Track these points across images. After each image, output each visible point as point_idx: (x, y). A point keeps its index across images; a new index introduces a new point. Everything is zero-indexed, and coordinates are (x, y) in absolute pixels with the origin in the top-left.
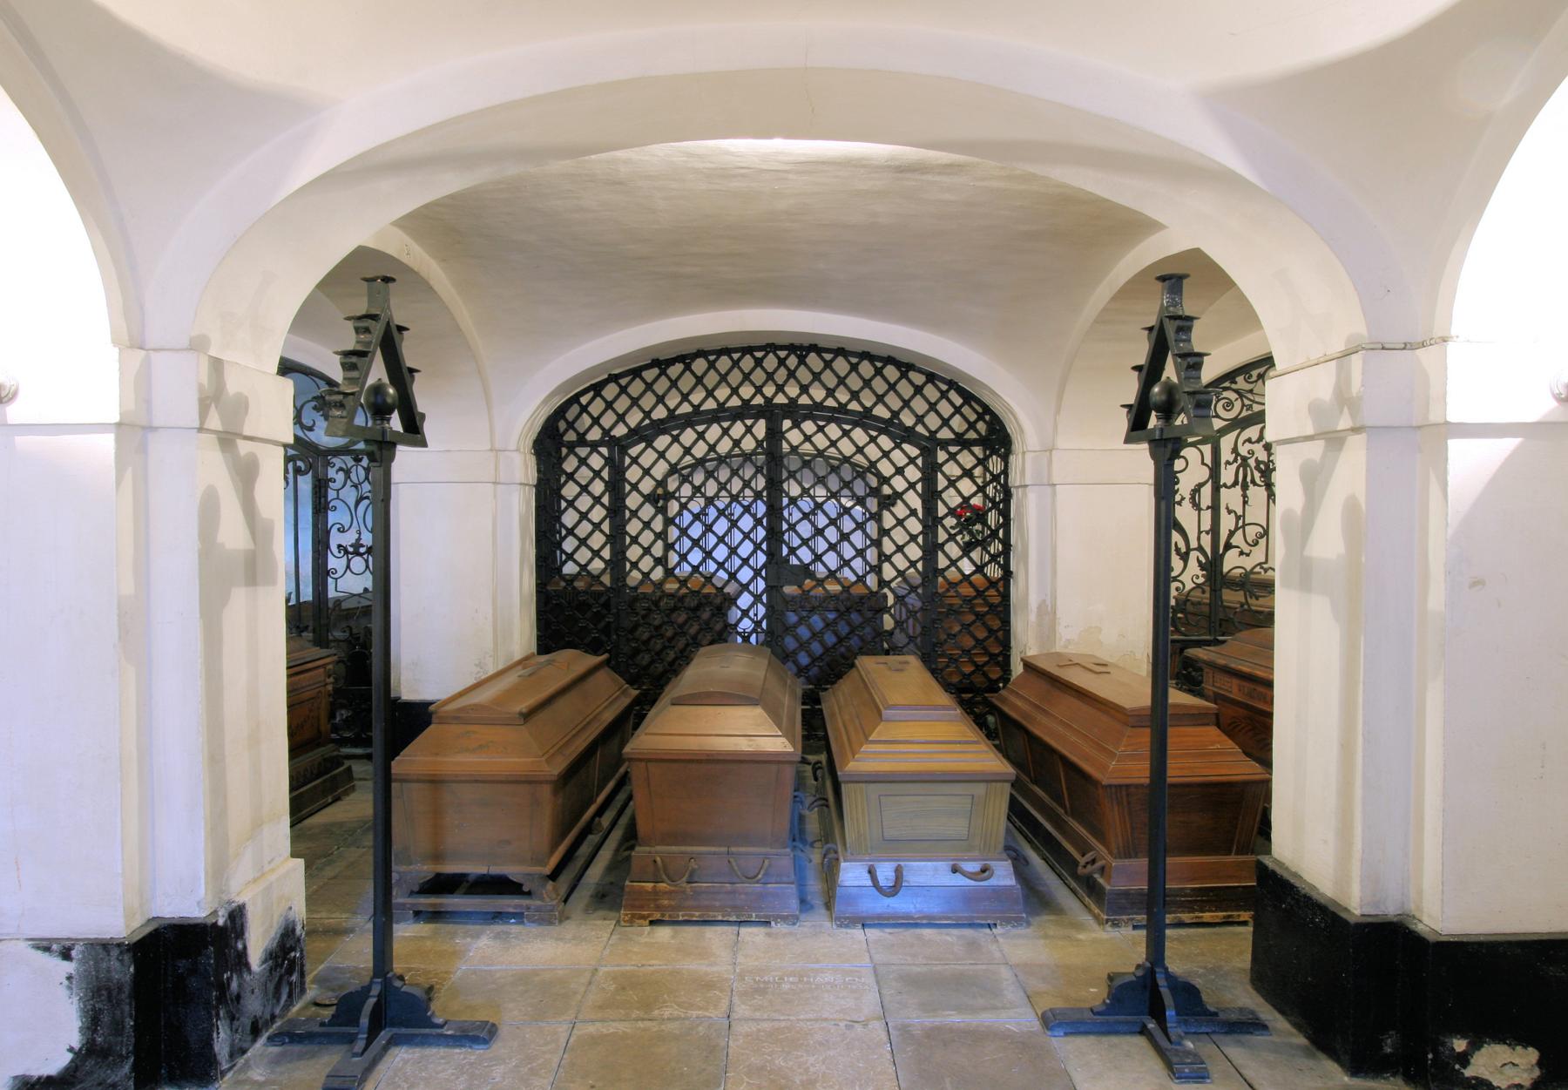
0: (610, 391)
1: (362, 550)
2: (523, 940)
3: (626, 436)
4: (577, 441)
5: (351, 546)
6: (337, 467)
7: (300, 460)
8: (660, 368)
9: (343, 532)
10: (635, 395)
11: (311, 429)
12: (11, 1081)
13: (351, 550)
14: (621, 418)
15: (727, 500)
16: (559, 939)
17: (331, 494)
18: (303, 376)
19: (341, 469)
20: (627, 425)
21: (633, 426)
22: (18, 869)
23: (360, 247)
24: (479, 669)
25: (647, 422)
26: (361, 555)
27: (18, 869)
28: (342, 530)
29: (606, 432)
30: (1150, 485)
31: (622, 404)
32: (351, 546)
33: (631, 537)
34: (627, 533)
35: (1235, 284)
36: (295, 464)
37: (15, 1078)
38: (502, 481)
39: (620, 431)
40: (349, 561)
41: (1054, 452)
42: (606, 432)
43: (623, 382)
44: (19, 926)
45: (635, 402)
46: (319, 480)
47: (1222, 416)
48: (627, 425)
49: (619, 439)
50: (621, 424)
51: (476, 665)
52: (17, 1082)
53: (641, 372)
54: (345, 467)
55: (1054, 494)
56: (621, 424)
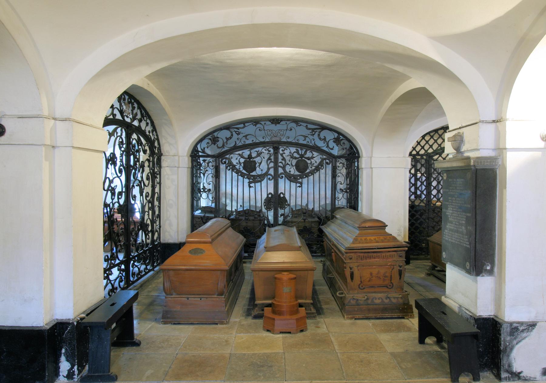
0: (427, 138)
1: (206, 190)
2: (54, 321)
3: (433, 153)
4: (416, 154)
5: (344, 189)
6: (339, 162)
7: (328, 160)
8: (444, 130)
9: (341, 184)
10: (436, 139)
11: (332, 149)
12: (542, 370)
13: (344, 190)
14: (431, 146)
15: (437, 174)
16: (57, 319)
17: (338, 171)
18: (329, 131)
19: (341, 163)
20: (433, 149)
21: (435, 149)
22: (543, 298)
23: (133, 85)
24: (398, 231)
25: (439, 148)
26: (205, 192)
27: (543, 298)
28: (341, 184)
29: (426, 151)
30: (163, 167)
31: (431, 142)
32: (344, 189)
33: (433, 187)
34: (425, 186)
35: (436, 98)
36: (326, 161)
37: (544, 368)
38: (180, 166)
39: (430, 151)
40: (343, 194)
41: (372, 158)
42: (426, 151)
43: (432, 134)
44: (543, 317)
45: (436, 141)
46: (159, 164)
47: (222, 141)
48: (433, 149)
49: (430, 154)
50: (431, 149)
51: (398, 230)
52: (544, 370)
53: (438, 131)
54: (342, 162)
55: (372, 171)
56: (431, 149)
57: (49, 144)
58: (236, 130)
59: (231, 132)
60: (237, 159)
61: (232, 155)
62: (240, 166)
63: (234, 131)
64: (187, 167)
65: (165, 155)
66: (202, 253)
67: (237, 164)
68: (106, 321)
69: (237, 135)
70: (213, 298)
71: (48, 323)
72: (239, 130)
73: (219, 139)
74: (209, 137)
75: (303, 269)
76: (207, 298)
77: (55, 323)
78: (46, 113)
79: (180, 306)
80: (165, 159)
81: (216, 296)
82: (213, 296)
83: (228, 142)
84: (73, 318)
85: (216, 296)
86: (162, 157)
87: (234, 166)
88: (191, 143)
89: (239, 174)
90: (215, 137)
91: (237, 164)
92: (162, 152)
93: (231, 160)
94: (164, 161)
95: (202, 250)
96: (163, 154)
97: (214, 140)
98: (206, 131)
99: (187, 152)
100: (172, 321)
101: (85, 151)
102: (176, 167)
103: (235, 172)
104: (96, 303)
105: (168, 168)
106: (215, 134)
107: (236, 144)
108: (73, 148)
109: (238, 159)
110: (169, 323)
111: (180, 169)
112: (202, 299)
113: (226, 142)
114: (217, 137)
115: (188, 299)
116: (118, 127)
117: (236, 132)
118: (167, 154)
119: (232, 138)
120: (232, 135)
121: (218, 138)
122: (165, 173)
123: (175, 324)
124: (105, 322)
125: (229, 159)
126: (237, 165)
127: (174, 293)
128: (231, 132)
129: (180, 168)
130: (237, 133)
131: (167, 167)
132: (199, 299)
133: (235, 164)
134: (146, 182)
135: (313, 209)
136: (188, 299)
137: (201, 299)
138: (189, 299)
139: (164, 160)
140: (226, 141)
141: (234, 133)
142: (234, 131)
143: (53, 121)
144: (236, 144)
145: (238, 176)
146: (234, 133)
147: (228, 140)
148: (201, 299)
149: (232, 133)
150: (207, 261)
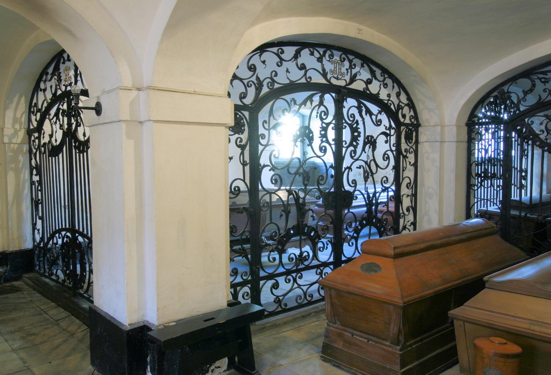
16: (148, 322)
57: (129, 119)
58: (541, 76)
59: (533, 81)
60: (541, 124)
61: (532, 119)
62: (547, 135)
63: (538, 78)
64: (456, 141)
65: (424, 125)
66: (376, 271)
67: (542, 132)
68: (162, 341)
69: (543, 84)
70: (383, 344)
71: (135, 323)
72: (547, 75)
73: (511, 95)
74: (495, 94)
75: (538, 338)
76: (376, 342)
77: (142, 324)
78: (128, 83)
79: (342, 343)
80: (423, 132)
81: (388, 343)
82: (384, 342)
83: (526, 97)
84: (157, 325)
85: (388, 343)
86: (419, 128)
87: (537, 136)
88: (461, 106)
89: (546, 148)
90: (505, 93)
91: (542, 132)
92: (420, 122)
93: (532, 126)
94: (423, 134)
95: (378, 266)
96: (422, 125)
97: (503, 97)
98: (483, 86)
99: (456, 118)
100: (334, 361)
101: (193, 125)
102: (437, 141)
103: (537, 146)
104: (208, 312)
105: (427, 143)
106: (505, 88)
107: (540, 98)
108: (153, 122)
109: (544, 125)
110: (329, 362)
111: (446, 144)
112: (370, 342)
113: (524, 98)
114: (508, 92)
115: (353, 336)
116: (313, 95)
117: (540, 79)
118: (427, 124)
119: (534, 89)
120: (534, 85)
121: (511, 93)
122: (424, 151)
123: (334, 365)
124: (161, 341)
125: (529, 126)
126: (540, 135)
127: (338, 323)
128: (533, 81)
129: (446, 143)
130: (543, 80)
131: (427, 142)
132: (366, 341)
133: (538, 132)
134: (382, 163)
135: (263, 211)
136: (353, 336)
137: (368, 342)
138: (354, 336)
139: (422, 132)
140: (523, 96)
141: (537, 82)
142: (538, 78)
143: (135, 93)
144: (540, 98)
145: (543, 152)
146: (537, 82)
147: (527, 94)
148: (368, 342)
149: (535, 81)
150: (377, 286)
